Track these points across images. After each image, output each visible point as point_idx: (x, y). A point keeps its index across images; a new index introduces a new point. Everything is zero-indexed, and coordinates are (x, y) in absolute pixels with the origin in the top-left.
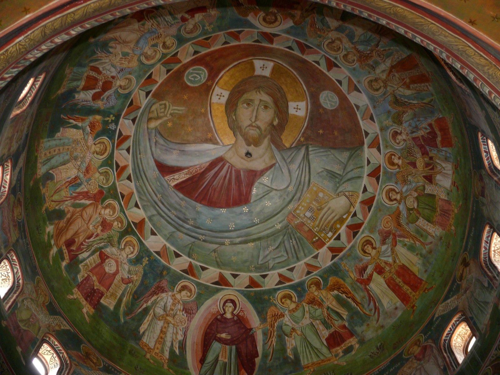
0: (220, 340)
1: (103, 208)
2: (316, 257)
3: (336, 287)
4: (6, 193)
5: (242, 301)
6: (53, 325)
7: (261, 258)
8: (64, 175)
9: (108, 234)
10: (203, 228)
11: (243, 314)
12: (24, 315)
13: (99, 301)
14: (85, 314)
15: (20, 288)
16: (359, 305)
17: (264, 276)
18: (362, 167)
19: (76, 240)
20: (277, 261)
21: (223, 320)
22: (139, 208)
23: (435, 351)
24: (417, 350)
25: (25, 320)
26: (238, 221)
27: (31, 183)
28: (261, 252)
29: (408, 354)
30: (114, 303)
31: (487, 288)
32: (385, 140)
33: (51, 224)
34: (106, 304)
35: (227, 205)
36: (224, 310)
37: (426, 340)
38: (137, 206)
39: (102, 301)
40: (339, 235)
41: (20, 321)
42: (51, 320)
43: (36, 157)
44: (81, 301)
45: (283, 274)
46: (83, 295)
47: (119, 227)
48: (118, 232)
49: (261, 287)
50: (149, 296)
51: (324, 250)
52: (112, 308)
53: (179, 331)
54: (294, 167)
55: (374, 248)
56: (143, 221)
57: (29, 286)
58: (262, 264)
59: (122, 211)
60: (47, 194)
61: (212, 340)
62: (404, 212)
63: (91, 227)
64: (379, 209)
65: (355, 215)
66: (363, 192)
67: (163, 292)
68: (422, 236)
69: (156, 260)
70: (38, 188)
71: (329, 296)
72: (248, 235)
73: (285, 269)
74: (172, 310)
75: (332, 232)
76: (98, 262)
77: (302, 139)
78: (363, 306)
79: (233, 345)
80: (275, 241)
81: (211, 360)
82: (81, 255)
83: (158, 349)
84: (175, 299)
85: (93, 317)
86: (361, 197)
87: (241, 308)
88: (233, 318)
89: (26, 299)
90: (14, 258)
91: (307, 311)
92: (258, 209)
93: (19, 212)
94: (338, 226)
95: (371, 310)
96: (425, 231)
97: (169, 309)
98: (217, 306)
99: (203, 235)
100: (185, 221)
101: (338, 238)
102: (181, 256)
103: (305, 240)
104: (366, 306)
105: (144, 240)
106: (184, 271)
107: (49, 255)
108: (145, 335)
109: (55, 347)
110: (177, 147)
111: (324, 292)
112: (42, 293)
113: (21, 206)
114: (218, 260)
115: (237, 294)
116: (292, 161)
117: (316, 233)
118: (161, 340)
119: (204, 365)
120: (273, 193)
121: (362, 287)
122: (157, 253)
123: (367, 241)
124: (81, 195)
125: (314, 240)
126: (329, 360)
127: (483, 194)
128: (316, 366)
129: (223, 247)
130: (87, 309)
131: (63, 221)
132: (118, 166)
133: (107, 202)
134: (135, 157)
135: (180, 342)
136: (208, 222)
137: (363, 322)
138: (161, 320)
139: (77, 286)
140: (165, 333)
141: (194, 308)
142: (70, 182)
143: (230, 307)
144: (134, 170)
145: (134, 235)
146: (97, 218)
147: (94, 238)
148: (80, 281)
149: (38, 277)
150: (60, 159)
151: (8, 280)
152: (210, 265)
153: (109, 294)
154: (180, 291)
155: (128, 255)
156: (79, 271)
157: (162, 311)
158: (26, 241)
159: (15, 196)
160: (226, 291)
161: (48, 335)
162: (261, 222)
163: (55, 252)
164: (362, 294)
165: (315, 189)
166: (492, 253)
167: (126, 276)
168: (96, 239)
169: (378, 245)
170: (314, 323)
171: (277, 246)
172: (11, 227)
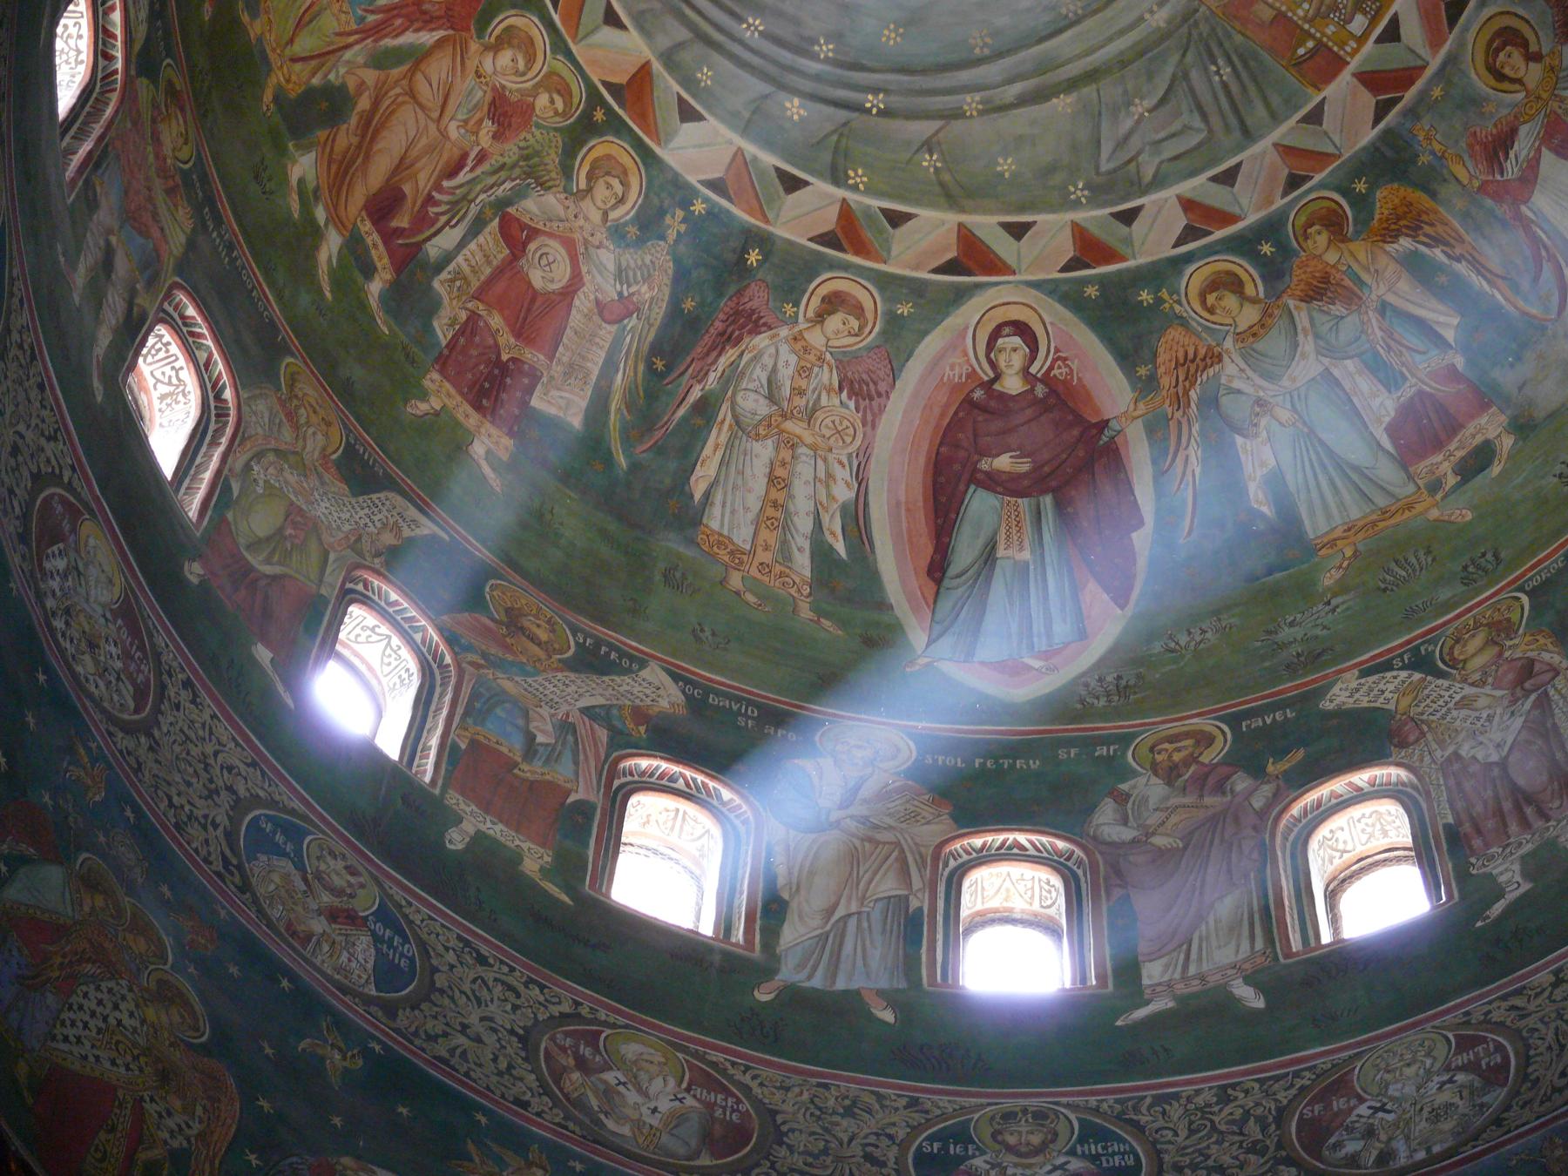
0: (993, 482)
1: (487, 48)
2: (1315, 117)
3: (1402, 223)
4: (119, 76)
6: (372, 529)
7: (1106, 149)
9: (522, 144)
10: (869, 64)
11: (1064, 370)
13: (524, 404)
14: (484, 464)
15: (232, 419)
16: (1500, 282)
17: (1128, 217)
20: (1170, 150)
21: (993, 404)
22: (622, 26)
25: (268, 539)
28: (1105, 126)
30: (582, 403)
33: (307, 149)
34: (553, 411)
36: (993, 365)
39: (535, 402)
40: (1395, 22)
41: (248, 547)
42: (362, 513)
44: (460, 417)
45: (1198, 199)
46: (462, 394)
47: (556, 113)
48: (556, 129)
49: (1123, 259)
50: (708, 354)
52: (576, 421)
53: (837, 466)
55: (1536, 57)
56: (643, 75)
58: (1115, 170)
59: (561, 47)
60: (270, 38)
61: (962, 487)
63: (453, 131)
67: (756, 331)
69: (713, 214)
70: (236, 21)
72: (1043, 67)
73: (1202, 179)
75: (1365, 13)
76: (500, 257)
78: (1516, 289)
79: (1044, 492)
80: (1150, 76)
81: (969, 560)
82: (435, 241)
83: (766, 548)
84: (806, 350)
87: (1057, 350)
88: (1032, 389)
89: (259, 456)
90: (191, 311)
91: (1304, 329)
97: (786, 391)
98: (966, 354)
99: (875, 91)
101: (1392, 34)
102: (806, 183)
103: (1267, 58)
104: (1525, 284)
105: (659, 144)
106: (827, 239)
107: (315, 267)
108: (712, 504)
109: (391, 610)
112: (314, 419)
113: (182, 109)
114: (946, 177)
115: (1033, 296)
117: (1306, 26)
118: (775, 512)
119: (946, 583)
122: (716, 186)
123: (1500, 33)
124: (398, 16)
125: (1301, 51)
126: (1410, 507)
128: (1361, 536)
129: (957, 126)
131: (345, 126)
133: (498, 26)
135: (844, 509)
138: (766, 437)
139: (437, 360)
140: (786, 485)
141: (883, 371)
143: (1015, 350)
145: (617, 134)
146: (470, 93)
147: (472, 170)
148: (444, 343)
149: (290, 360)
151: (180, 397)
152: (918, 202)
153: (557, 369)
154: (820, 317)
155: (605, 214)
156: (433, 307)
157: (763, 401)
158: (221, 236)
160: (992, 291)
161: (358, 573)
163: (335, 250)
167: (610, 290)
168: (478, 171)
170: (1336, 372)
171: (1161, 93)
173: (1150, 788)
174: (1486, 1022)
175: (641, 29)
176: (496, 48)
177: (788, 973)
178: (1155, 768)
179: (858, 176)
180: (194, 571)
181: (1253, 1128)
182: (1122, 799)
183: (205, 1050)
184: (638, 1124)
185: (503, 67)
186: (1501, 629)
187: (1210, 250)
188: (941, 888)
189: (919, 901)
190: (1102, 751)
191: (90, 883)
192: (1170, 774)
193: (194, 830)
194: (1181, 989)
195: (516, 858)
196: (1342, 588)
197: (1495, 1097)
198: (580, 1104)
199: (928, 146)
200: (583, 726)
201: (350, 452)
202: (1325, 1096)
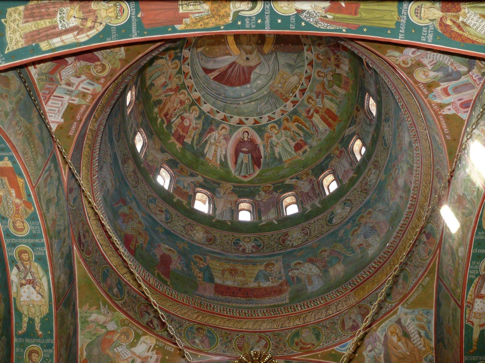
0: (243, 152)
2: (285, 106)
5: (251, 131)
8: (159, 82)
12: (150, 158)
13: (183, 141)
17: (261, 118)
18: (304, 61)
19: (169, 113)
23: (346, 153)
24: (337, 152)
26: (246, 92)
27: (145, 90)
29: (334, 154)
31: (369, 125)
33: (156, 108)
35: (240, 85)
37: (341, 147)
38: (196, 91)
39: (185, 140)
40: (296, 95)
43: (145, 77)
51: (289, 103)
52: (190, 143)
54: (271, 63)
56: (199, 98)
57: (151, 142)
59: (189, 94)
60: (152, 93)
62: (327, 83)
63: (175, 105)
64: (314, 81)
65: (302, 84)
66: (306, 73)
67: (213, 131)
68: (336, 94)
69: (208, 116)
71: (293, 125)
73: (270, 113)
74: (219, 139)
77: (273, 49)
85: (182, 149)
86: (305, 75)
89: (150, 149)
92: (255, 85)
93: (141, 107)
94: (295, 90)
95: (314, 131)
96: (337, 91)
99: (229, 101)
100: (220, 95)
101: (295, 96)
106: (222, 120)
110: (212, 59)
111: (291, 123)
115: (249, 128)
116: (269, 60)
118: (215, 155)
120: (262, 76)
121: (309, 120)
127: (364, 77)
130: (178, 146)
132: (184, 73)
133: (181, 91)
134: (192, 67)
136: (231, 94)
137: (311, 137)
142: (163, 85)
144: (192, 74)
150: (156, 75)
153: (188, 136)
154: (221, 130)
156: (172, 128)
159: (138, 100)
162: (257, 91)
164: (309, 123)
165: (282, 73)
166: (370, 106)
167: (195, 126)
169: (315, 99)
172: (139, 115)
173: (263, 193)
175: (199, 92)
176: (181, 94)
177: (217, 218)
179: (227, 111)
180: (142, 165)
185: (182, 97)
189: (233, 208)
192: (265, 192)
195: (183, 202)
197: (307, 237)
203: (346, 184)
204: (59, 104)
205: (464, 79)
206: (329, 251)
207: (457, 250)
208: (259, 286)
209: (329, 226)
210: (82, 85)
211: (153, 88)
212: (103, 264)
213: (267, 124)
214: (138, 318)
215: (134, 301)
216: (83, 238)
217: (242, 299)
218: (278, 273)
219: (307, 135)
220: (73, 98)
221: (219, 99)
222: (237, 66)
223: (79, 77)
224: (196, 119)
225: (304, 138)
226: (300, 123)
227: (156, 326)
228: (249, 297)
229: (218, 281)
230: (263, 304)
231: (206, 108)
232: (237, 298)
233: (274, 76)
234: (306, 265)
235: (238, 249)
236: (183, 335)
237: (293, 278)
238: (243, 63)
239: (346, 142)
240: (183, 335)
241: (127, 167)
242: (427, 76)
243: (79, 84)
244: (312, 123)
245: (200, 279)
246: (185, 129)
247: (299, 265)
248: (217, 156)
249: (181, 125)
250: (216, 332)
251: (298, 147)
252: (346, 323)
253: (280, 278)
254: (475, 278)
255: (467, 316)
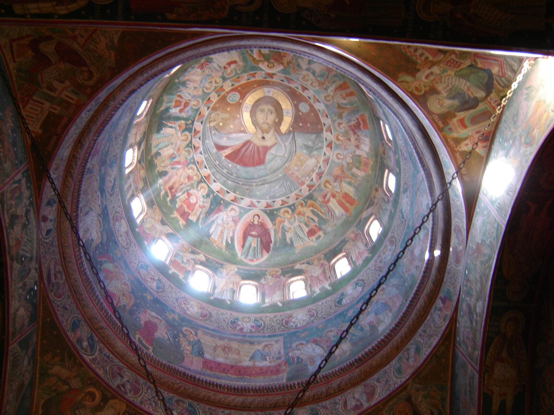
0: (252, 236)
2: (301, 190)
7: (272, 192)
13: (188, 218)
17: (274, 202)
19: (175, 186)
20: (281, 193)
24: (353, 236)
32: (334, 128)
35: (253, 165)
39: (189, 218)
43: (151, 144)
51: (305, 186)
54: (287, 144)
56: (209, 176)
59: (198, 170)
63: (182, 180)
65: (320, 167)
69: (217, 195)
72: (264, 180)
74: (226, 221)
78: (325, 215)
86: (323, 158)
101: (312, 180)
106: (232, 201)
120: (277, 158)
121: (325, 205)
129: (252, 187)
142: (170, 156)
144: (203, 149)
153: (193, 214)
154: (230, 211)
156: (176, 203)
167: (201, 204)
173: (269, 277)
174: (312, 309)
175: (209, 169)
176: (189, 169)
177: (215, 296)
178: (270, 275)
179: (237, 192)
180: (137, 230)
181: (278, 321)
182: (265, 278)
183: (130, 292)
184: (191, 313)
185: (190, 172)
186: (319, 259)
187: (285, 207)
188: (238, 288)
189: (235, 288)
190: (263, 272)
191: (116, 267)
192: (272, 276)
193: (133, 263)
194: (271, 303)
195: (179, 276)
196: (298, 253)
197: (312, 319)
198: (184, 309)
199: (248, 190)
200: (191, 260)
201: (162, 219)
202: (289, 318)
203: (359, 265)
204: (37, 110)
205: (481, 107)
206: (335, 331)
207: (475, 307)
208: (254, 364)
209: (337, 306)
210: (65, 92)
211: (159, 157)
212: (74, 313)
213: (280, 209)
214: (108, 378)
215: (106, 360)
216: (54, 278)
217: (233, 376)
218: (277, 353)
219: (323, 221)
220: (55, 106)
221: (230, 179)
222: (252, 145)
223: (63, 82)
224: (203, 197)
225: (319, 224)
226: (315, 208)
227: (128, 391)
228: (241, 375)
229: (207, 356)
230: (257, 383)
231: (216, 186)
232: (228, 375)
233: (290, 158)
234: (309, 346)
235: (236, 328)
236: (159, 405)
237: (293, 359)
238: (258, 142)
239: (362, 223)
240: (159, 405)
241: (118, 226)
242: (442, 105)
243: (62, 91)
244: (328, 208)
245: (188, 352)
246: (191, 206)
247: (301, 346)
248: (223, 237)
249: (187, 201)
250: (198, 407)
251: (311, 233)
252: (349, 403)
253: (279, 358)
254: (458, 153)
255: (486, 382)
